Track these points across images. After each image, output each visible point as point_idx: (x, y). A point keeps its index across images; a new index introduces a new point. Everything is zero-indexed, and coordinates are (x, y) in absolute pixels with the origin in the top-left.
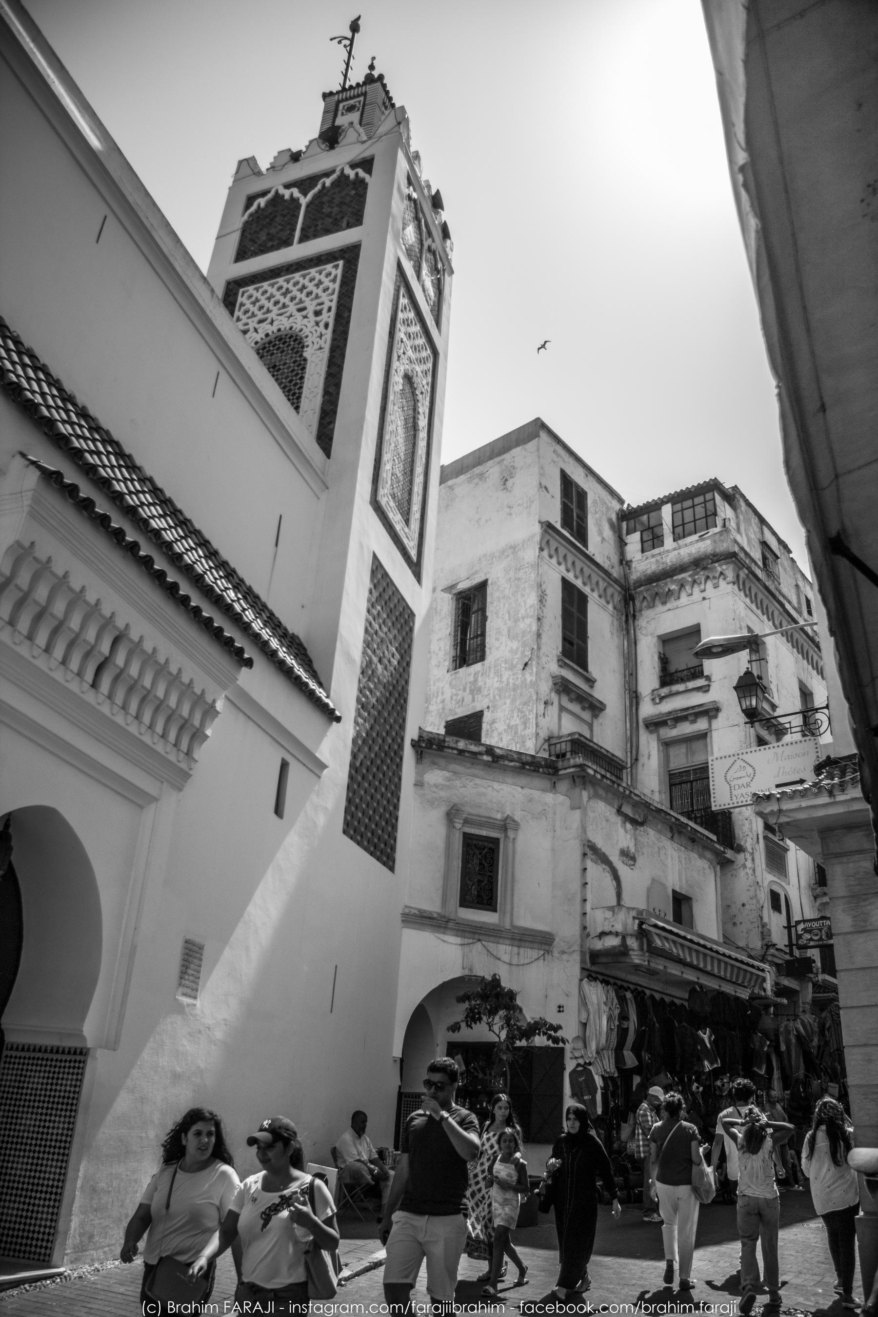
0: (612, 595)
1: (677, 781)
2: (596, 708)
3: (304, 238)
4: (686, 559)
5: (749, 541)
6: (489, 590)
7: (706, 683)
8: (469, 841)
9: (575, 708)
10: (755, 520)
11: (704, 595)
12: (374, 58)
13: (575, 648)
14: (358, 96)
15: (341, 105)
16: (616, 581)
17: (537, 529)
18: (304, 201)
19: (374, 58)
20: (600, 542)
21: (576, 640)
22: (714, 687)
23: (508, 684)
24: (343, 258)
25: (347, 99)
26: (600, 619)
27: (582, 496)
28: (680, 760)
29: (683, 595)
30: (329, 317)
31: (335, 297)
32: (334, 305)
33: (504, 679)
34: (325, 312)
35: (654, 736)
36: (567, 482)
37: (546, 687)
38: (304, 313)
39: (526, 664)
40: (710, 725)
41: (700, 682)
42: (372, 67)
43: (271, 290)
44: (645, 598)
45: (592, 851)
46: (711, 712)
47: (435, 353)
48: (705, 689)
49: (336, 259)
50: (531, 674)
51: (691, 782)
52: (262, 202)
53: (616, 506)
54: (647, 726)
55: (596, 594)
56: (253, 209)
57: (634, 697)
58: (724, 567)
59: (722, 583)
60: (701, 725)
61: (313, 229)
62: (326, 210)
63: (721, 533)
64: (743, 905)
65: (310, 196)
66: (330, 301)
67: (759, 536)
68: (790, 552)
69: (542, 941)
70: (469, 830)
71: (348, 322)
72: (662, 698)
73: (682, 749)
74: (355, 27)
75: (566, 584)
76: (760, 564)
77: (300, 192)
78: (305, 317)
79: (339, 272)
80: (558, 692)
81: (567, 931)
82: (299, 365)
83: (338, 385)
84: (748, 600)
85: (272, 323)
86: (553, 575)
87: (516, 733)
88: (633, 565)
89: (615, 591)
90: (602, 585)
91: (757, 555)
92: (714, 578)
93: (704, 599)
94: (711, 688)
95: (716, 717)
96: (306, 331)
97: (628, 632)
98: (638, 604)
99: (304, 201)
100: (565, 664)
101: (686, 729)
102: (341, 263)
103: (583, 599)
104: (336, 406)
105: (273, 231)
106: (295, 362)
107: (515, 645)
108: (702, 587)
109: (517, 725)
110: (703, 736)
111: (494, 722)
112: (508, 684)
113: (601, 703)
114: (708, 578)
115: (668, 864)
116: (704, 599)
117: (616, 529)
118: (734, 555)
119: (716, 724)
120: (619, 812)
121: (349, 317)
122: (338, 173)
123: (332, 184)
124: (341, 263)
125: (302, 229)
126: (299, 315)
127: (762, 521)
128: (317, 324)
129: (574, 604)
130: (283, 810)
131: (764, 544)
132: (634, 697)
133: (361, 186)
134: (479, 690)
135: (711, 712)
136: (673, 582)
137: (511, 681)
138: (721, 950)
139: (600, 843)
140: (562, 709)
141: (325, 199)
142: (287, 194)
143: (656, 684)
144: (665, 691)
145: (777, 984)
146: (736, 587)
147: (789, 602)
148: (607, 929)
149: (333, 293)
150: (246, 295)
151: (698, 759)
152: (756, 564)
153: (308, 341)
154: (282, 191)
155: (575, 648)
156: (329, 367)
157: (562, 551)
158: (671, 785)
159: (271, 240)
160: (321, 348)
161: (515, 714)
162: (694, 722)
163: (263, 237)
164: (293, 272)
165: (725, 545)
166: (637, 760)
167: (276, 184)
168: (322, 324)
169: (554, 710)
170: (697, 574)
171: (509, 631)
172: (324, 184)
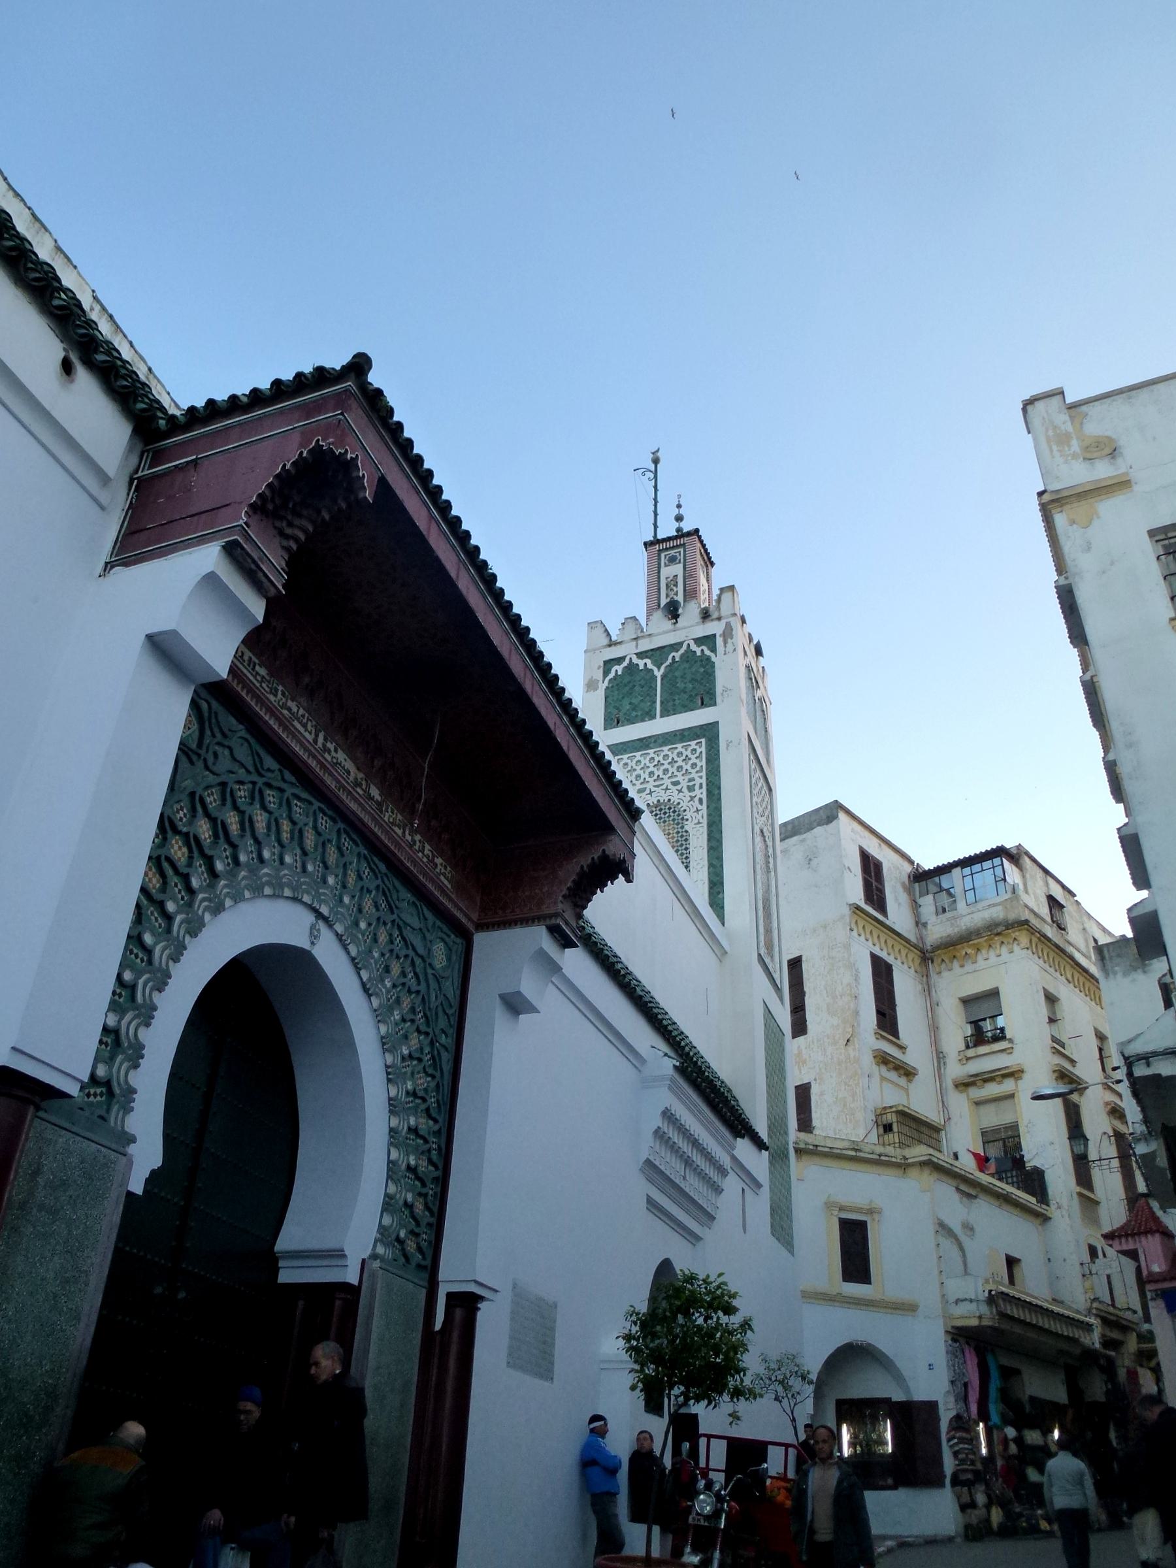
2: (908, 1073)
3: (666, 713)
5: (1036, 898)
6: (805, 966)
9: (893, 1075)
10: (1040, 873)
12: (679, 496)
13: (887, 1019)
14: (678, 546)
15: (663, 555)
16: (915, 946)
17: (847, 911)
18: (658, 674)
19: (679, 496)
20: (898, 914)
21: (887, 1012)
24: (704, 736)
25: (667, 549)
26: (905, 984)
27: (878, 866)
28: (993, 1118)
29: (980, 958)
30: (702, 793)
31: (704, 774)
32: (704, 781)
34: (697, 787)
35: (964, 1095)
36: (866, 858)
37: (868, 1060)
38: (679, 787)
42: (679, 518)
45: (943, 1228)
47: (770, 790)
49: (698, 737)
50: (854, 1050)
52: (619, 669)
53: (908, 868)
55: (899, 962)
57: (940, 1058)
59: (1016, 948)
60: (1008, 1086)
61: (671, 703)
62: (680, 685)
66: (701, 779)
67: (1045, 889)
68: (1074, 895)
69: (907, 1308)
70: (845, 1215)
71: (719, 799)
72: (968, 1059)
74: (656, 461)
75: (875, 959)
76: (1049, 919)
77: (654, 663)
78: (680, 791)
79: (703, 749)
80: (878, 1064)
81: (928, 1298)
83: (720, 858)
84: (1041, 961)
85: (651, 793)
86: (861, 951)
87: (845, 1105)
88: (929, 927)
89: (914, 955)
90: (904, 952)
91: (1044, 911)
94: (1015, 1051)
95: (1021, 1078)
96: (684, 805)
99: (658, 674)
101: (992, 1089)
102: (703, 740)
103: (889, 968)
104: (722, 878)
105: (634, 701)
106: (678, 832)
107: (835, 1021)
111: (822, 1094)
113: (914, 1068)
115: (996, 1229)
117: (909, 891)
118: (1026, 922)
120: (957, 1189)
121: (720, 794)
122: (685, 647)
123: (682, 656)
124: (703, 740)
125: (662, 702)
126: (674, 788)
127: (1046, 872)
128: (692, 798)
129: (882, 973)
130: (1016, 1281)
131: (1051, 900)
132: (940, 1058)
133: (708, 667)
134: (804, 1062)
136: (969, 947)
138: (1051, 1307)
139: (947, 1221)
140: (883, 1078)
141: (677, 674)
142: (641, 663)
144: (971, 1053)
145: (1103, 1336)
146: (1029, 952)
147: (1078, 950)
148: (961, 1297)
149: (701, 771)
151: (1007, 1119)
152: (1043, 920)
153: (688, 815)
154: (635, 660)
155: (887, 1019)
156: (709, 840)
157: (869, 928)
159: (634, 709)
160: (699, 823)
162: (1000, 1083)
163: (626, 706)
164: (661, 746)
167: (628, 650)
168: (696, 799)
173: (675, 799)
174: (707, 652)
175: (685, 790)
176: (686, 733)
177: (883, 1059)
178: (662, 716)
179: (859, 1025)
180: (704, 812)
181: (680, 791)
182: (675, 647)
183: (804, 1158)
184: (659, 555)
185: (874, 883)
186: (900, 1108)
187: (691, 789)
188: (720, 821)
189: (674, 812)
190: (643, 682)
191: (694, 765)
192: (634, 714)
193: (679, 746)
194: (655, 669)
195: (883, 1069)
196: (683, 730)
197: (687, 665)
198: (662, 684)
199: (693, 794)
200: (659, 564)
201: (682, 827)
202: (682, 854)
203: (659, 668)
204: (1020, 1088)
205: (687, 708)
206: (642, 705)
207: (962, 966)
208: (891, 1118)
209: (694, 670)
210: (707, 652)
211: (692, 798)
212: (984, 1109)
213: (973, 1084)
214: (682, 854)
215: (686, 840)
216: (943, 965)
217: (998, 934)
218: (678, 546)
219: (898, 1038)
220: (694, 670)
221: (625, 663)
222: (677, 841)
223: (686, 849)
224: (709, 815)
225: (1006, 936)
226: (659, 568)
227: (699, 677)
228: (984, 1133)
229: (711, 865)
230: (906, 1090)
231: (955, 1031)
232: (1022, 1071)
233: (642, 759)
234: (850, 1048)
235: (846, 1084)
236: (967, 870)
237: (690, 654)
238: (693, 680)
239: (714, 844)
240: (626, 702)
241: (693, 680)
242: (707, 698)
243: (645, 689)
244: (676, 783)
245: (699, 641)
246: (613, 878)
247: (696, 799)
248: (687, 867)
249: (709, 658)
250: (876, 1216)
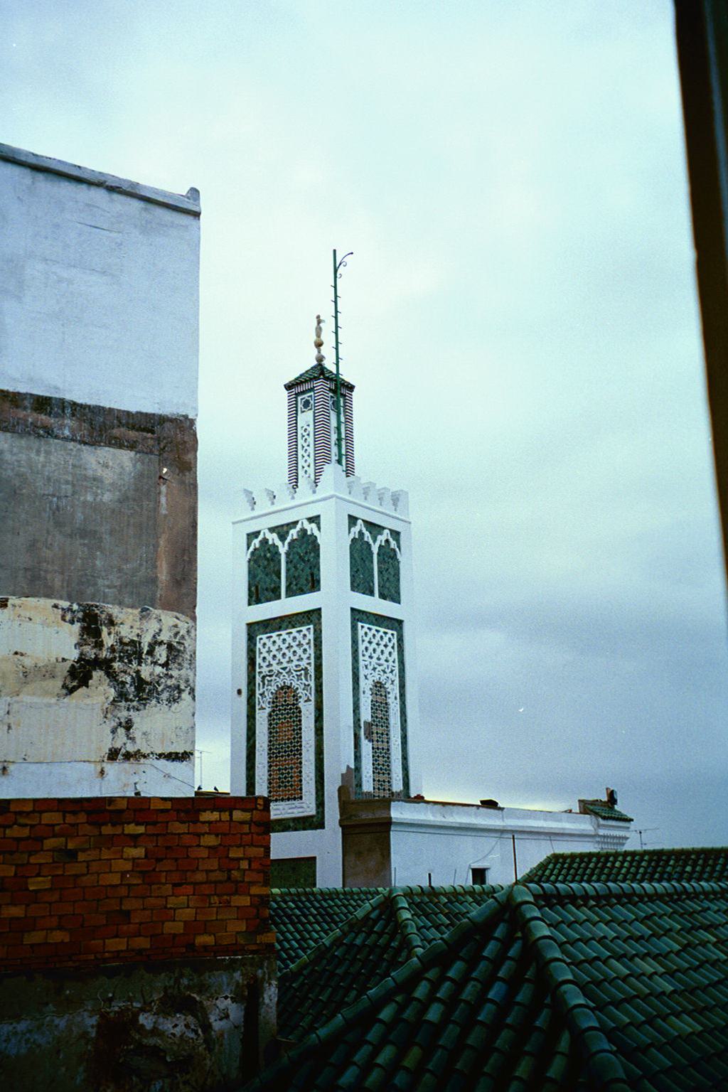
15: (299, 398)
18: (283, 549)
56: (251, 549)
99: (283, 549)
102: (311, 626)
124: (311, 626)
221: (261, 537)
245: (311, 520)
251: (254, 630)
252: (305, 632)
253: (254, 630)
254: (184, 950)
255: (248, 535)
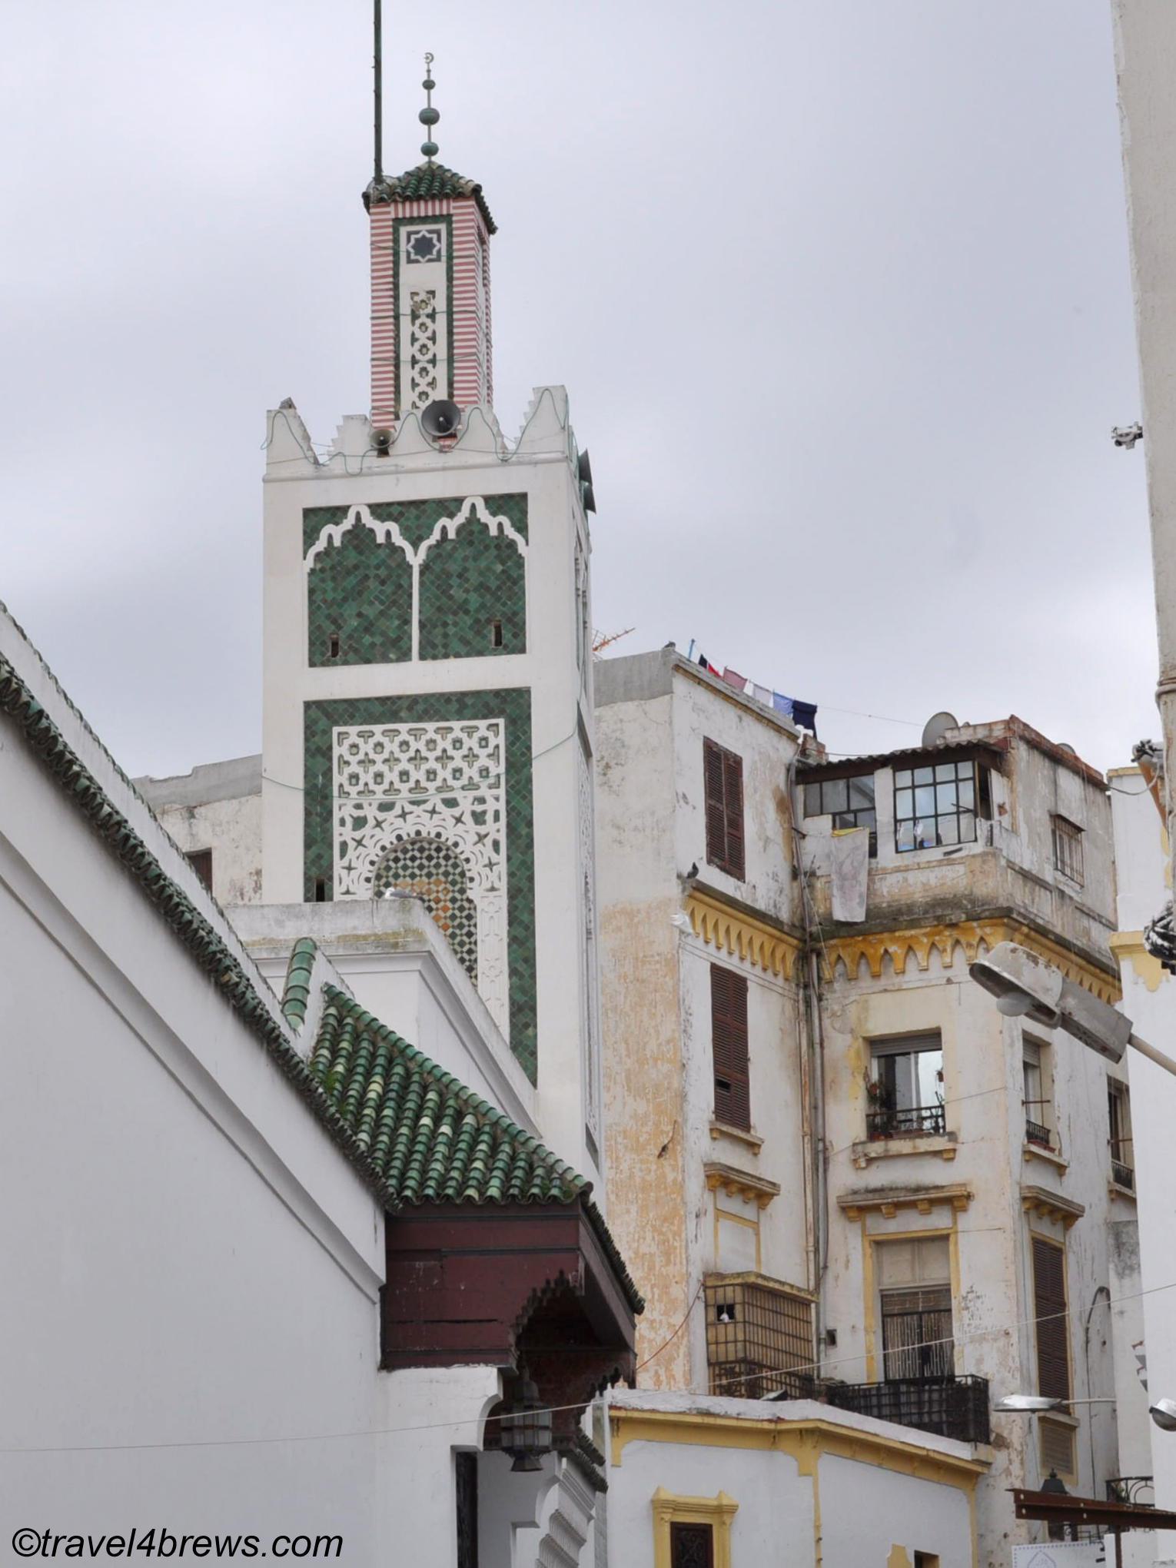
0: (784, 958)
1: (896, 1309)
4: (919, 897)
7: (950, 1146)
8: (677, 1529)
9: (734, 1205)
11: (949, 973)
12: (430, 58)
14: (435, 219)
15: (403, 231)
18: (416, 559)
19: (430, 58)
22: (963, 1151)
23: (631, 1176)
25: (412, 220)
26: (766, 1015)
28: (902, 1274)
29: (911, 966)
30: (498, 830)
31: (502, 792)
32: (502, 806)
33: (624, 1166)
34: (489, 817)
35: (856, 1228)
38: (456, 811)
39: (664, 1149)
40: (955, 1222)
41: (939, 1143)
43: (391, 747)
44: (839, 957)
46: (956, 1201)
48: (946, 1156)
51: (920, 1314)
52: (334, 532)
54: (844, 1209)
55: (758, 970)
56: (320, 545)
58: (988, 930)
60: (939, 1220)
61: (439, 630)
63: (984, 854)
64: (1005, 1536)
65: (424, 545)
66: (496, 801)
72: (870, 1161)
73: (905, 1255)
77: (406, 532)
79: (501, 740)
80: (712, 1189)
82: (461, 909)
87: (651, 1268)
92: (970, 945)
93: (949, 981)
95: (964, 1209)
97: (809, 1020)
98: (825, 966)
99: (416, 559)
100: (722, 1133)
102: (501, 722)
105: (370, 612)
106: (454, 900)
107: (641, 1107)
108: (947, 960)
109: (652, 1255)
110: (942, 1239)
112: (631, 1176)
114: (957, 942)
116: (949, 981)
117: (785, 805)
119: (965, 1221)
124: (501, 722)
128: (481, 838)
129: (729, 994)
135: (956, 1201)
137: (638, 1173)
140: (720, 1213)
142: (380, 528)
143: (860, 1131)
144: (876, 1148)
150: (347, 743)
151: (932, 1275)
156: (510, 924)
158: (884, 1316)
160: (493, 889)
161: (649, 1235)
162: (927, 1212)
164: (420, 719)
165: (991, 883)
166: (826, 1267)
168: (488, 841)
169: (708, 1220)
170: (939, 933)
171: (628, 1079)
172: (444, 529)
173: (450, 834)
174: (510, 532)
175: (468, 818)
176: (469, 701)
177: (722, 1180)
178: (422, 657)
179: (685, 1121)
180: (503, 868)
181: (459, 820)
182: (449, 506)
183: (624, 1430)
184: (396, 233)
185: (723, 807)
186: (752, 1279)
187: (479, 818)
188: (531, 890)
189: (447, 858)
190: (383, 572)
191: (484, 772)
192: (367, 639)
193: (456, 725)
194: (718, 805)
195: (721, 1194)
196: (464, 694)
197: (469, 551)
198: (422, 584)
199: (482, 830)
200: (396, 254)
201: (462, 891)
202: (462, 944)
203: (415, 545)
204: (960, 1227)
205: (472, 650)
206: (382, 623)
207: (876, 976)
208: (733, 1295)
209: (483, 564)
210: (510, 532)
211: (481, 838)
212: (888, 1256)
213: (876, 1208)
214: (462, 944)
215: (469, 917)
216: (840, 968)
217: (953, 926)
218: (435, 219)
219: (747, 1127)
220: (483, 564)
221: (348, 523)
222: (453, 917)
223: (470, 934)
224: (511, 875)
225: (965, 931)
226: (396, 263)
227: (493, 584)
228: (885, 1297)
229: (513, 972)
230: (756, 1226)
231: (847, 1117)
232: (969, 1197)
233: (385, 741)
234: (666, 1162)
235: (654, 1228)
236: (905, 778)
237: (476, 528)
238: (482, 587)
239: (520, 932)
240: (350, 610)
241: (482, 587)
242: (505, 633)
243: (389, 589)
244: (451, 803)
245: (498, 503)
246: (614, 1380)
247: (488, 841)
248: (470, 969)
249: (512, 545)
250: (726, 1518)
251: (323, 717)
252: (483, 732)
253: (323, 717)
254: (676, 1085)
255: (308, 513)
